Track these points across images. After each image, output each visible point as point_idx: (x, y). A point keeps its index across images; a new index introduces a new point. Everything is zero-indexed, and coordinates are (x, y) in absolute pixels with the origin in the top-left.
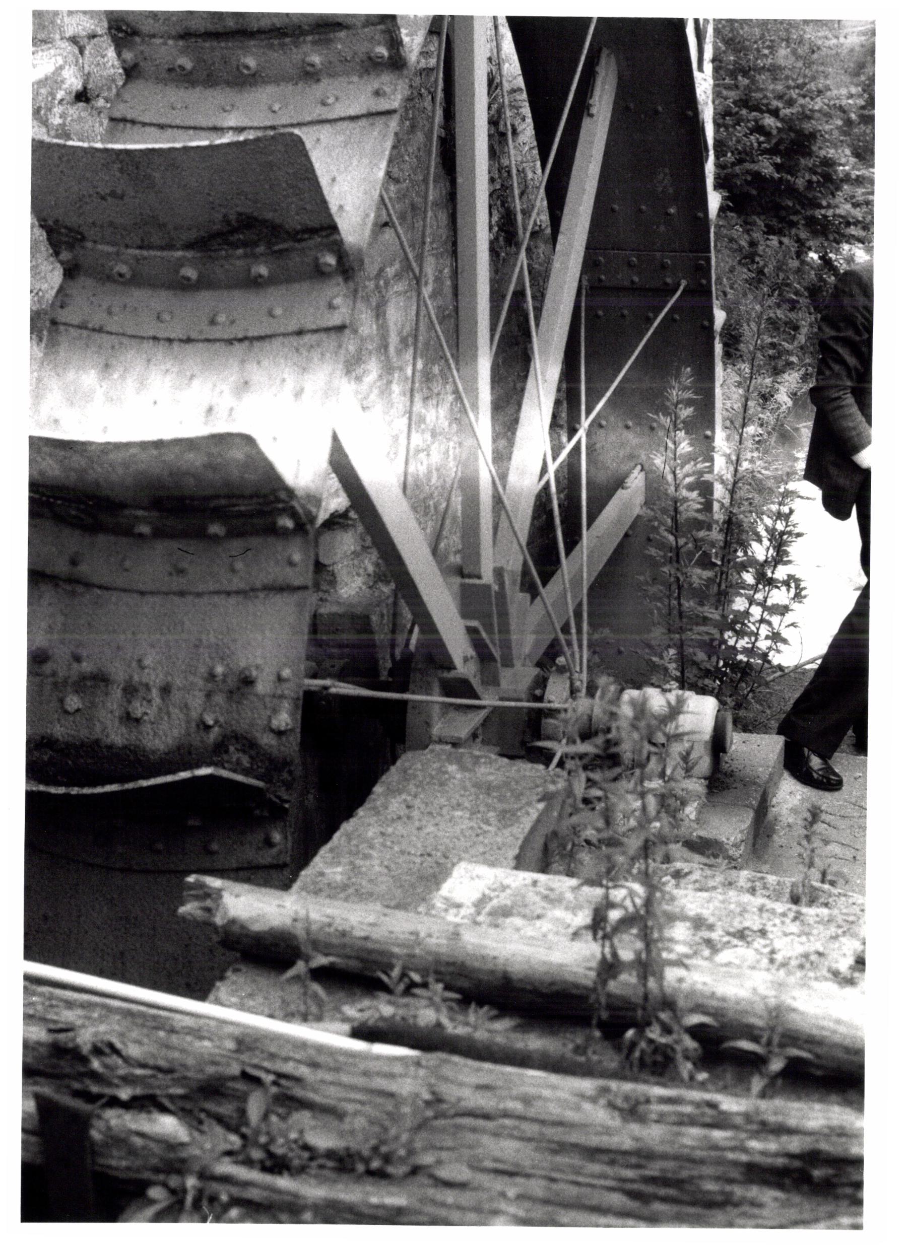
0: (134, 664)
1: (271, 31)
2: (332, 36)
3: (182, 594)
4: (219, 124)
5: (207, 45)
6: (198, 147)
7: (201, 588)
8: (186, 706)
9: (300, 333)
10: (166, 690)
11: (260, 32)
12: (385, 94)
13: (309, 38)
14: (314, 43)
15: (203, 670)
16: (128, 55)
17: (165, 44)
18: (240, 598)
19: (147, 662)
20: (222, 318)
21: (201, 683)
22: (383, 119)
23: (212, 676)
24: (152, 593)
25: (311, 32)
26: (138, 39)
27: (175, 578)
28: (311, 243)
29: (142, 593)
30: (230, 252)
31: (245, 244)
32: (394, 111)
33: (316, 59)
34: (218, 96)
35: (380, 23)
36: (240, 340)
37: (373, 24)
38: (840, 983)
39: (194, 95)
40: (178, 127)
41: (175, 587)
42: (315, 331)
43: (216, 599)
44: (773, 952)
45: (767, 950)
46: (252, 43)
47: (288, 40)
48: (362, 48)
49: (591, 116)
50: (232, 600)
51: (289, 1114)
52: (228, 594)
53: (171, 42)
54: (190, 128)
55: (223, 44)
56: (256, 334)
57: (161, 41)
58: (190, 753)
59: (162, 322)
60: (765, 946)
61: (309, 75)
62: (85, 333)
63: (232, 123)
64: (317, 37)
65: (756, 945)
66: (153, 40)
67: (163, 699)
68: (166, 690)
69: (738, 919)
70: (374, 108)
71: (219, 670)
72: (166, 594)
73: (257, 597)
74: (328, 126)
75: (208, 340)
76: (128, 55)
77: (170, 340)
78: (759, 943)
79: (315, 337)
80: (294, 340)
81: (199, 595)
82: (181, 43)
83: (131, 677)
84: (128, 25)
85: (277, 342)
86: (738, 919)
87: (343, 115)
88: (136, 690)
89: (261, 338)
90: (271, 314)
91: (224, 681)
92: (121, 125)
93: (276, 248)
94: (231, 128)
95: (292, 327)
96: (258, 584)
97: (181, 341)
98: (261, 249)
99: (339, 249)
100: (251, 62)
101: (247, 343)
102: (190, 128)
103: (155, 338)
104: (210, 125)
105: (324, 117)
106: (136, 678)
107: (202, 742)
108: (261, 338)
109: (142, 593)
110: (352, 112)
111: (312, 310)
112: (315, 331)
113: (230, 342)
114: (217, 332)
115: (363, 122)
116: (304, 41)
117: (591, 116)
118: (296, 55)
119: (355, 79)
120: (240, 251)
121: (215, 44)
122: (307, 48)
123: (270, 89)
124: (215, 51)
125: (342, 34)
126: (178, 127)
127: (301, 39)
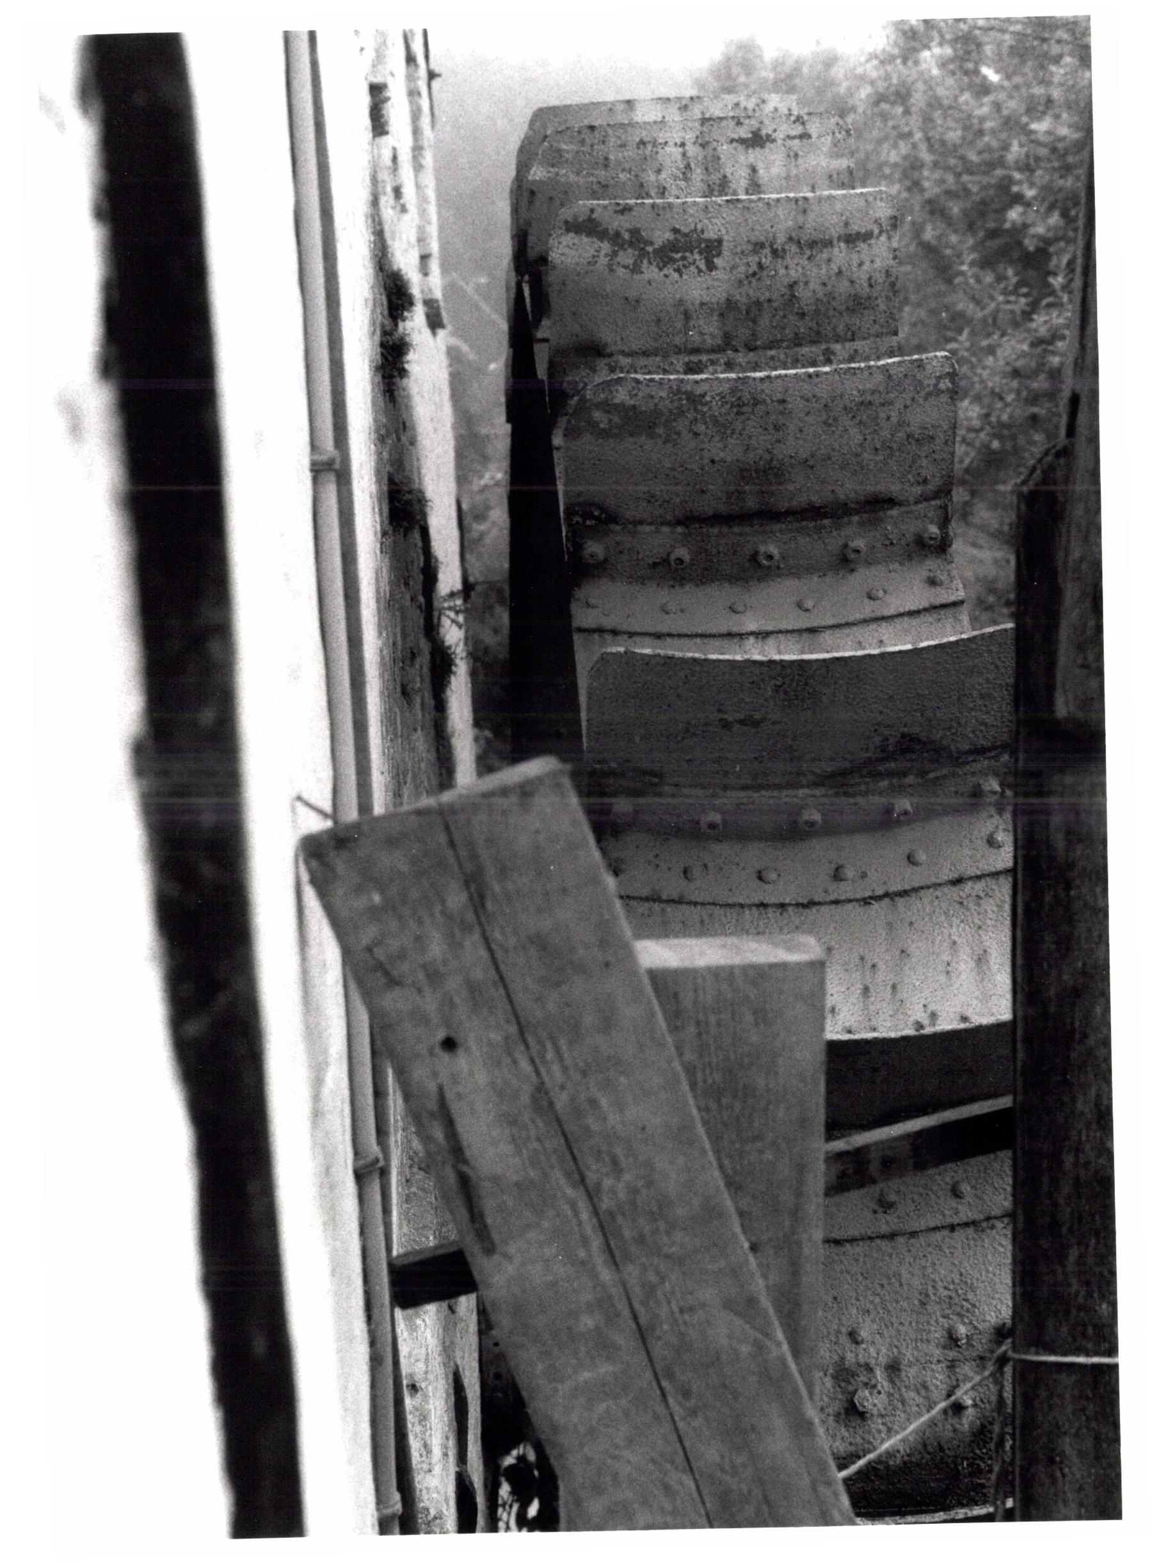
0: (844, 1340)
1: (803, 511)
2: (881, 514)
3: (892, 1236)
4: (735, 630)
5: (715, 530)
6: (900, 652)
7: (915, 1225)
8: (925, 1386)
9: (958, 881)
10: (893, 1368)
11: (790, 513)
12: (941, 584)
13: (856, 518)
14: (861, 524)
15: (938, 1335)
17: (657, 531)
18: (970, 1231)
19: (864, 1334)
20: (850, 873)
21: (937, 1352)
22: (949, 612)
23: (952, 1340)
24: (852, 1240)
25: (857, 512)
26: (613, 527)
27: (881, 1215)
28: (977, 766)
30: (872, 786)
31: (891, 774)
32: (962, 602)
33: (860, 543)
34: (719, 595)
35: (934, 499)
36: (879, 898)
37: (926, 500)
39: (687, 595)
40: (680, 636)
41: (884, 1229)
42: (978, 878)
43: (937, 1236)
46: (778, 526)
47: (826, 522)
48: (911, 528)
50: (959, 1235)
52: (952, 1228)
53: (666, 529)
54: (696, 635)
55: (736, 530)
56: (900, 888)
57: (653, 528)
58: (941, 1449)
59: (766, 883)
61: (845, 562)
62: (657, 907)
63: (752, 626)
64: (865, 516)
66: (639, 528)
67: (892, 1381)
68: (893, 1368)
71: (962, 1330)
72: (871, 1238)
73: (993, 1227)
74: (884, 624)
75: (836, 902)
77: (783, 906)
79: (979, 886)
80: (953, 893)
81: (913, 1234)
82: (679, 529)
83: (843, 1359)
84: (602, 509)
85: (927, 896)
87: (901, 610)
88: (854, 1375)
89: (904, 893)
90: (911, 859)
91: (969, 1344)
92: (596, 636)
93: (932, 775)
94: (752, 633)
95: (946, 875)
97: (798, 905)
98: (910, 779)
100: (774, 550)
101: (887, 900)
102: (696, 635)
103: (763, 905)
104: (724, 630)
105: (878, 614)
106: (850, 1357)
107: (955, 1430)
108: (904, 893)
110: (911, 606)
111: (967, 852)
112: (978, 878)
113: (866, 901)
114: (844, 890)
115: (929, 618)
116: (850, 523)
118: (834, 541)
119: (897, 566)
120: (884, 784)
121: (725, 529)
122: (848, 531)
123: (791, 583)
124: (720, 538)
125: (894, 512)
126: (680, 636)
127: (846, 519)
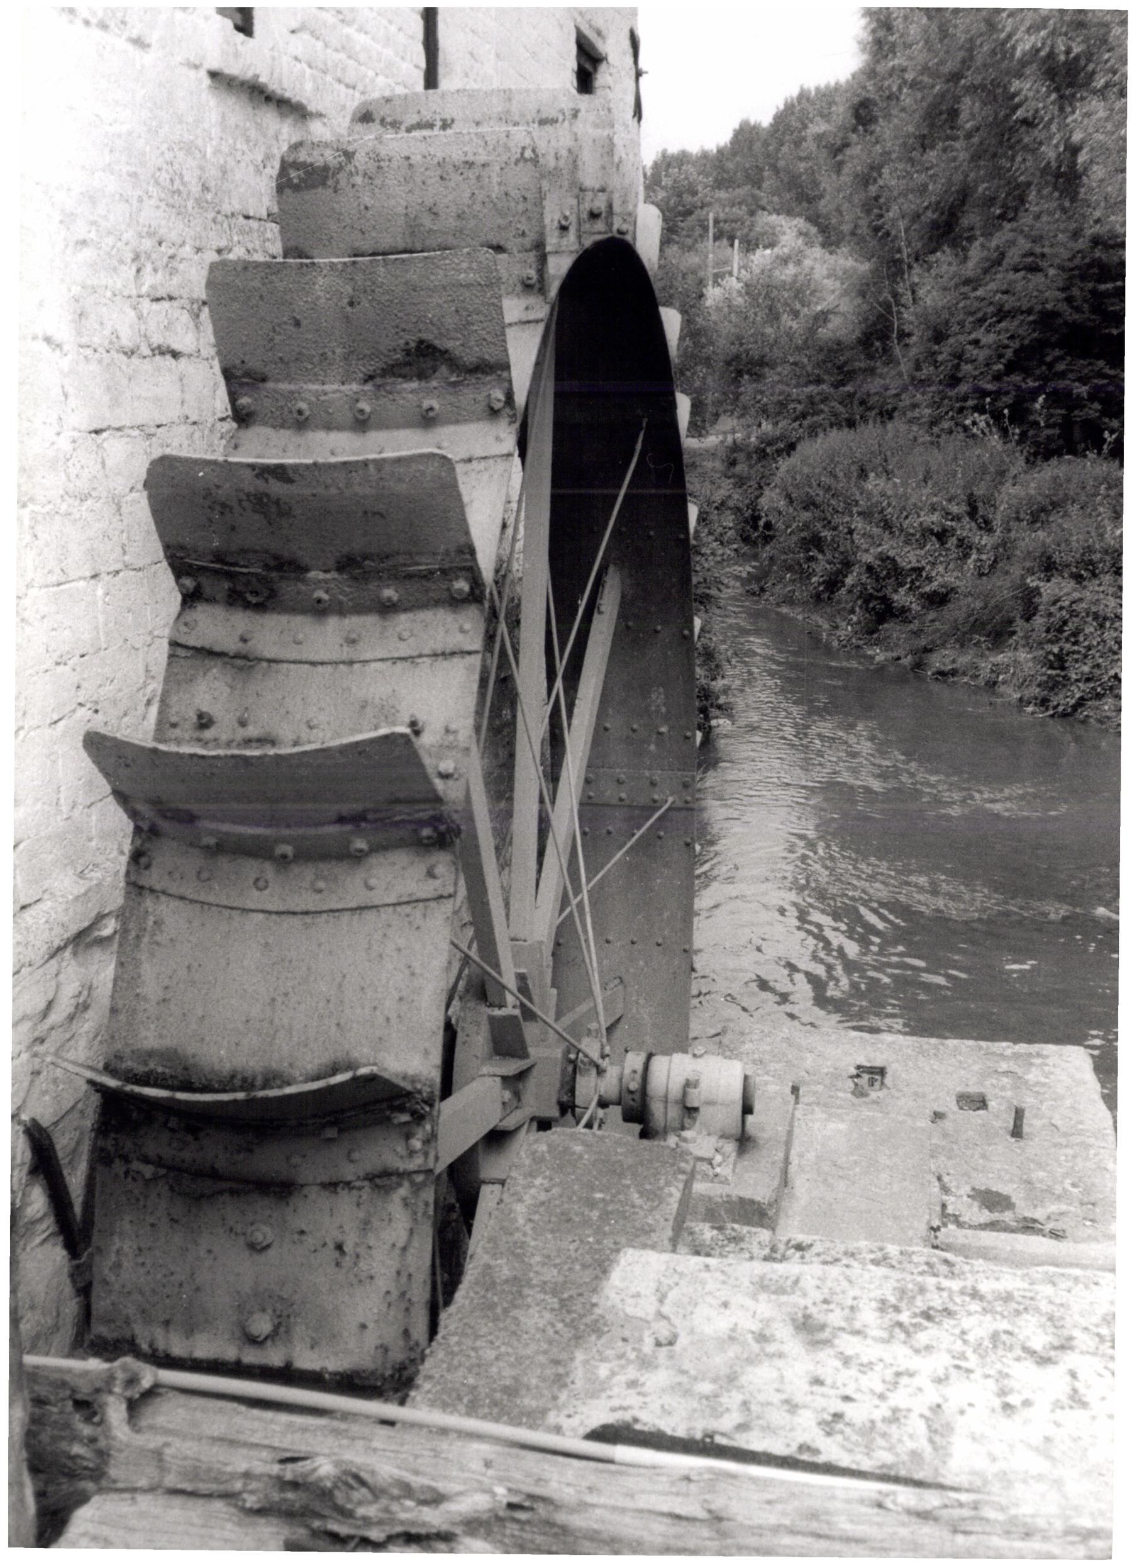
7: (368, 656)
16: (34, 1428)
18: (406, 665)
24: (322, 663)
29: (313, 664)
38: (1038, 1363)
41: (345, 657)
44: (963, 1333)
45: (957, 1331)
49: (600, 613)
51: (429, 1217)
60: (955, 1326)
65: (946, 1326)
69: (919, 1298)
70: (525, 319)
76: (34, 1428)
78: (948, 1323)
79: (483, 465)
86: (919, 1298)
96: (426, 651)
99: (476, 581)
109: (313, 664)
117: (600, 613)
